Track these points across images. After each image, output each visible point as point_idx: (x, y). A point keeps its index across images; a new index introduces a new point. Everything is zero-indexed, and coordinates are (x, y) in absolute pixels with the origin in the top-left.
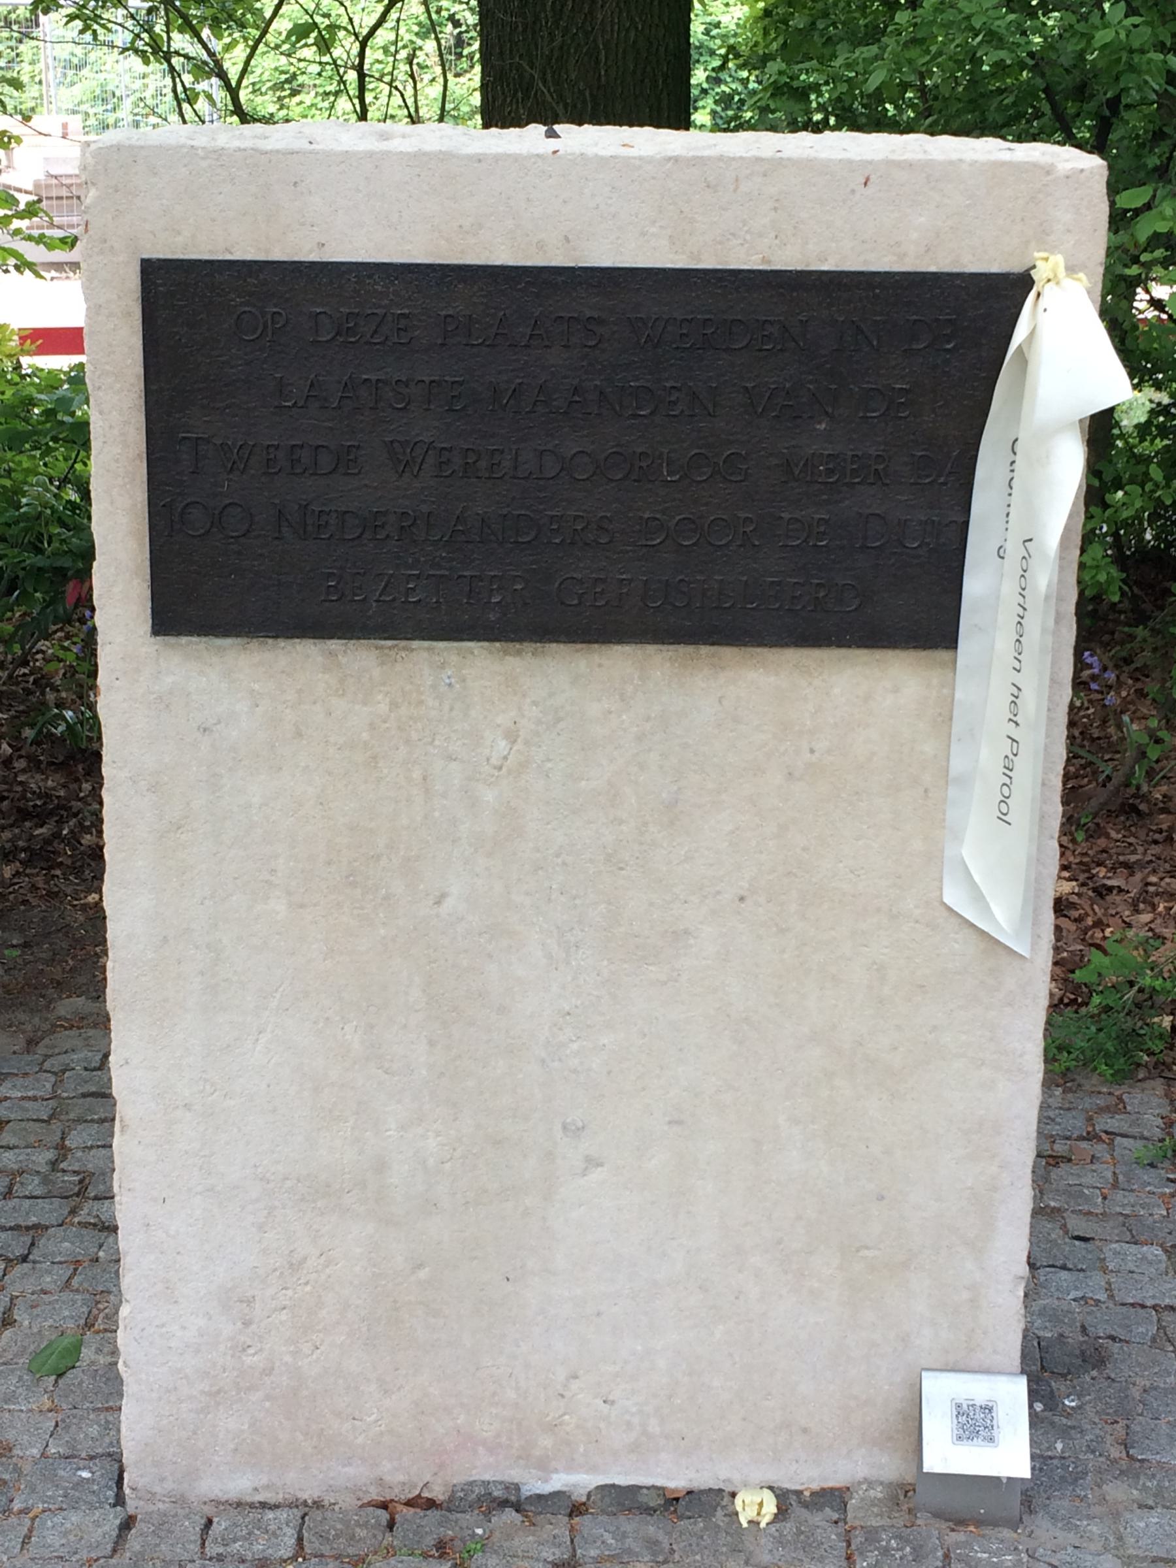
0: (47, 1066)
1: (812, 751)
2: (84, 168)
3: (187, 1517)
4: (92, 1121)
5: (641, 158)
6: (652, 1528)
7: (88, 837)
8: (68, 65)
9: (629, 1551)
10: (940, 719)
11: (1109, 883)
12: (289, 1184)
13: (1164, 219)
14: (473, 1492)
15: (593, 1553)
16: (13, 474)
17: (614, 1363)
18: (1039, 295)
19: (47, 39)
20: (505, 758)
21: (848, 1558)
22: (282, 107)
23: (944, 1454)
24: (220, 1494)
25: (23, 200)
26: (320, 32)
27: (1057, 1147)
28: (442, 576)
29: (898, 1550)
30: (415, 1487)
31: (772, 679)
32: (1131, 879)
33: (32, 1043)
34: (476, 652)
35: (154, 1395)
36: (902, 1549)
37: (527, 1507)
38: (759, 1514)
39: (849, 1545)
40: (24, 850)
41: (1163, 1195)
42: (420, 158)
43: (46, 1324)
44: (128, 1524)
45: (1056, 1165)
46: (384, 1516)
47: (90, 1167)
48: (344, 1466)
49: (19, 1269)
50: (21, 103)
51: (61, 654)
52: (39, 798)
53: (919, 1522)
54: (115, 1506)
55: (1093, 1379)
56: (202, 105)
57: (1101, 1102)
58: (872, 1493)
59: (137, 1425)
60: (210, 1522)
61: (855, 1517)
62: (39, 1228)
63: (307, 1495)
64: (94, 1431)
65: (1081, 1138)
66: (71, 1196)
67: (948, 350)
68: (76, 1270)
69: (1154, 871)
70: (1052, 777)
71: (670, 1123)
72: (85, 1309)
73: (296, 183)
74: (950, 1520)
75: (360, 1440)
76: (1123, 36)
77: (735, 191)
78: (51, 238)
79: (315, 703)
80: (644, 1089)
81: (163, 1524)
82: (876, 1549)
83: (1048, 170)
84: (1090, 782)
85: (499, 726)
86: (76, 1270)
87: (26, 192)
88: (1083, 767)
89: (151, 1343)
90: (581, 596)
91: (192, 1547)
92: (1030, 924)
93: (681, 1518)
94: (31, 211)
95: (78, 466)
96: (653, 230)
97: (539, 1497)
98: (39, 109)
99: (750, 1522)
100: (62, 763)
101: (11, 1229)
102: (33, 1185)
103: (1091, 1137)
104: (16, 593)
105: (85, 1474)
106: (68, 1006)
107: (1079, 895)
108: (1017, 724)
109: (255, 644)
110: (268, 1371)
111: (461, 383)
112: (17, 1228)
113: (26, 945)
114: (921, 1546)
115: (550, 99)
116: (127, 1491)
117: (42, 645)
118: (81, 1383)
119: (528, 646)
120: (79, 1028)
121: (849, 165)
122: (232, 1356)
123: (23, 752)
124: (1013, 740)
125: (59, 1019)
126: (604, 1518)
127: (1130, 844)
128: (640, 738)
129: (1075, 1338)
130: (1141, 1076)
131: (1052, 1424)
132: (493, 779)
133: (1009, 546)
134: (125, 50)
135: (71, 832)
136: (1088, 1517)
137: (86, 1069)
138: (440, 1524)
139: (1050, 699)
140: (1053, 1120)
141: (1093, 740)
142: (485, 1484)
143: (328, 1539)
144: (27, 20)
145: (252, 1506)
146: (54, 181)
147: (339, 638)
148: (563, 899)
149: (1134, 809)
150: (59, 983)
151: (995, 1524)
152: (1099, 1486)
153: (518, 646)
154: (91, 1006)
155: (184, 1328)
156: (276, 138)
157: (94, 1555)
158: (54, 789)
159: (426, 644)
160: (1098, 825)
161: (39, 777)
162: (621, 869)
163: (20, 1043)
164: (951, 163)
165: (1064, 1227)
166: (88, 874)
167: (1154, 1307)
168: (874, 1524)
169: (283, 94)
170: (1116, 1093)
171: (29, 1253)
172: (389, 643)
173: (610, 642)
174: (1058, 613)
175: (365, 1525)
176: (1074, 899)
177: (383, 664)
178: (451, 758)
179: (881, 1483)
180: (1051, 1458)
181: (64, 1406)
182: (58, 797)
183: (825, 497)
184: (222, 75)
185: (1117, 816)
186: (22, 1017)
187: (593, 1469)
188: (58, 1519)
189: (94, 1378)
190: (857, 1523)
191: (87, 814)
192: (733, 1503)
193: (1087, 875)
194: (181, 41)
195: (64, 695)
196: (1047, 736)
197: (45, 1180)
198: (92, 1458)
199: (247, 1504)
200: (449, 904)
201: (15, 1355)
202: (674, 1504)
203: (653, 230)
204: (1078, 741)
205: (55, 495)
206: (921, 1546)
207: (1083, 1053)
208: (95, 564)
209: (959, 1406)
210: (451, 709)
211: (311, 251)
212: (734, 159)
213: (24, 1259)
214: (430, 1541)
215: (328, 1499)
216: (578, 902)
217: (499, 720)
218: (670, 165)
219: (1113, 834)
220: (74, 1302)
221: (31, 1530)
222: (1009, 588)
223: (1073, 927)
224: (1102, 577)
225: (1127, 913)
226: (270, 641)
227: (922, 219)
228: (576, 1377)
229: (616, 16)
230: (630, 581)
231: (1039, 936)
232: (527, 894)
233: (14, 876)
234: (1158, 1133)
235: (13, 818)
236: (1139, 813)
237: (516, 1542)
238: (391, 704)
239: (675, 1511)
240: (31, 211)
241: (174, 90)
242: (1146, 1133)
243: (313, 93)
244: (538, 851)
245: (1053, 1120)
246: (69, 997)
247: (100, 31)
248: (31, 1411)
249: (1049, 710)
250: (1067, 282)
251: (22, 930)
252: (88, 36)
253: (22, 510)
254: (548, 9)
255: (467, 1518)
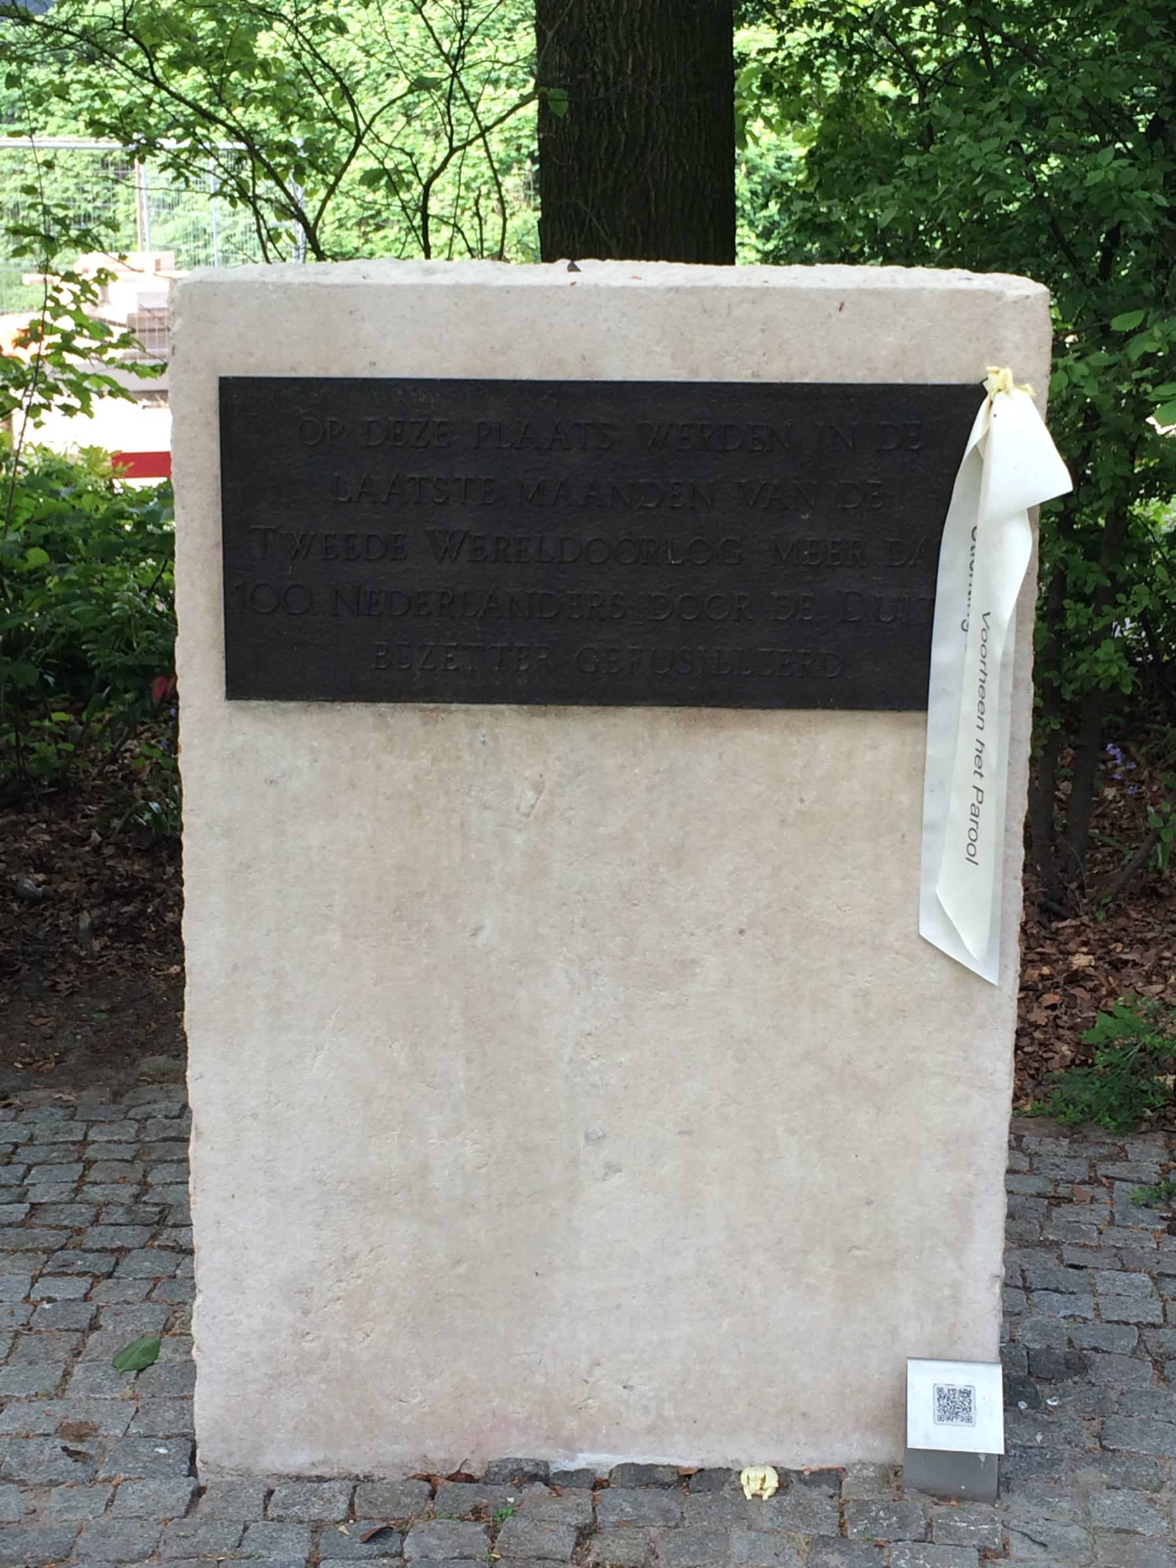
0: (131, 1114)
1: (802, 801)
2: (172, 301)
3: (252, 1485)
4: (172, 1161)
5: (646, 289)
6: (665, 1499)
7: (171, 915)
8: (162, 204)
9: (644, 1518)
10: (914, 773)
11: (1124, 957)
12: (343, 1186)
13: (1153, 340)
14: (506, 1467)
15: (612, 1519)
16: (105, 584)
17: (633, 1352)
18: (991, 403)
19: (143, 186)
20: (533, 806)
21: (841, 1526)
22: (367, 241)
23: (927, 1431)
24: (282, 1468)
25: (117, 332)
26: (390, 177)
27: (1059, 1189)
28: (477, 647)
29: (885, 1519)
30: (454, 1464)
31: (766, 737)
32: (1146, 954)
33: (117, 1095)
34: (506, 713)
35: (224, 1377)
36: (889, 1519)
37: (556, 1481)
38: (761, 1489)
39: (842, 1515)
40: (111, 925)
41: (1154, 1231)
42: (457, 290)
43: (129, 1328)
44: (199, 1492)
45: (1058, 1205)
46: (427, 1487)
47: (169, 1200)
48: (392, 1444)
49: (106, 1284)
50: (116, 241)
51: (147, 751)
52: (126, 880)
53: (906, 1497)
54: (188, 1476)
55: (1075, 1383)
56: (284, 242)
57: (1104, 1151)
58: (865, 1472)
59: (208, 1405)
60: (271, 1493)
61: (849, 1493)
62: (123, 1251)
63: (358, 1471)
64: (170, 1415)
65: (1083, 1182)
66: (152, 1224)
67: (913, 450)
68: (155, 1285)
69: (1169, 948)
70: (1015, 824)
71: (680, 1133)
72: (163, 1317)
73: (351, 312)
74: (934, 1496)
75: (406, 1421)
76: (1111, 176)
77: (728, 315)
78: (143, 366)
79: (366, 758)
80: (656, 1103)
81: (230, 1491)
82: (867, 1518)
83: (998, 296)
84: (1114, 868)
85: (527, 778)
86: (155, 1285)
87: (120, 325)
88: (1111, 855)
89: (221, 1329)
90: (597, 665)
91: (256, 1510)
92: (998, 953)
93: (691, 1492)
94: (125, 342)
95: (165, 576)
96: (658, 349)
97: (566, 1473)
98: (133, 247)
99: (753, 1495)
100: (148, 850)
101: (98, 1251)
102: (119, 1215)
103: (1093, 1181)
104: (107, 690)
105: (162, 1451)
106: (151, 1063)
107: (1095, 967)
108: (982, 775)
109: (314, 706)
110: (325, 1356)
111: (493, 481)
112: (103, 1250)
113: (112, 1010)
114: (907, 1517)
115: (602, 234)
116: (199, 1464)
117: (130, 744)
118: (160, 1375)
119: (552, 708)
120: (160, 1082)
121: (826, 293)
122: (293, 1342)
123: (111, 840)
124: (978, 790)
125: (143, 1074)
126: (623, 1491)
127: (1149, 923)
128: (650, 789)
129: (1061, 1349)
130: (1143, 1128)
131: (1035, 1420)
132: (522, 825)
133: (971, 620)
134: (214, 195)
135: (156, 910)
136: (1060, 1496)
137: (166, 1117)
138: (477, 1494)
139: (1011, 754)
140: (1058, 1167)
141: (1121, 830)
142: (518, 1461)
143: (376, 1505)
144: (122, 161)
145: (310, 1479)
146: (147, 315)
147: (388, 702)
148: (583, 931)
149: (1155, 892)
150: (142, 1043)
151: (974, 1499)
152: (1073, 1471)
153: (543, 708)
154: (172, 1064)
155: (250, 1316)
156: (336, 273)
157: (168, 1515)
158: (140, 872)
159: (464, 706)
160: (1119, 906)
161: (126, 862)
162: (636, 905)
163: (107, 1093)
164: (914, 291)
165: (1060, 1258)
166: (170, 948)
167: (1136, 1324)
168: (866, 1499)
169: (368, 229)
170: (1120, 1144)
171: (114, 1271)
172: (431, 706)
173: (623, 705)
174: (1015, 679)
175: (409, 1494)
176: (1091, 971)
177: (425, 724)
178: (485, 807)
179: (874, 1464)
180: (1031, 1447)
181: (144, 1395)
182: (143, 879)
183: (809, 578)
184: (301, 217)
185: (1138, 899)
186: (108, 1072)
187: (614, 1449)
188: (138, 1486)
189: (170, 1372)
190: (851, 1497)
191: (170, 894)
192: (739, 1480)
193: (1104, 950)
194: (264, 186)
195: (150, 789)
196: (1009, 787)
197: (129, 1211)
198: (168, 1438)
199: (305, 1477)
200: (484, 935)
201: (101, 1353)
202: (684, 1479)
203: (658, 349)
204: (1108, 831)
205: (144, 601)
206: (907, 1517)
207: (1089, 1106)
208: (178, 639)
209: (940, 1390)
210: (485, 763)
211: (364, 369)
212: (726, 288)
213: (110, 1275)
214: (467, 1507)
215: (378, 1473)
216: (597, 934)
217: (527, 773)
218: (672, 294)
219: (1134, 915)
220: (154, 1310)
221: (113, 1496)
222: (972, 657)
223: (1087, 996)
224: (1114, 671)
225: (1140, 984)
226: (328, 704)
227: (890, 339)
228: (599, 1364)
229: (665, 158)
230: (641, 651)
231: (1006, 967)
232: (553, 927)
233: (102, 949)
234: (1155, 1178)
235: (101, 899)
236: (1160, 897)
237: (543, 1509)
238: (433, 758)
239: (688, 1486)
240: (125, 342)
241: (259, 231)
242: (1144, 1179)
243: (396, 228)
244: (562, 888)
245: (1058, 1167)
246: (153, 1055)
247: (192, 178)
248: (113, 1399)
249: (1010, 764)
250: (1016, 392)
251: (108, 997)
252: (180, 184)
253: (114, 614)
254: (602, 152)
255: (499, 1490)
